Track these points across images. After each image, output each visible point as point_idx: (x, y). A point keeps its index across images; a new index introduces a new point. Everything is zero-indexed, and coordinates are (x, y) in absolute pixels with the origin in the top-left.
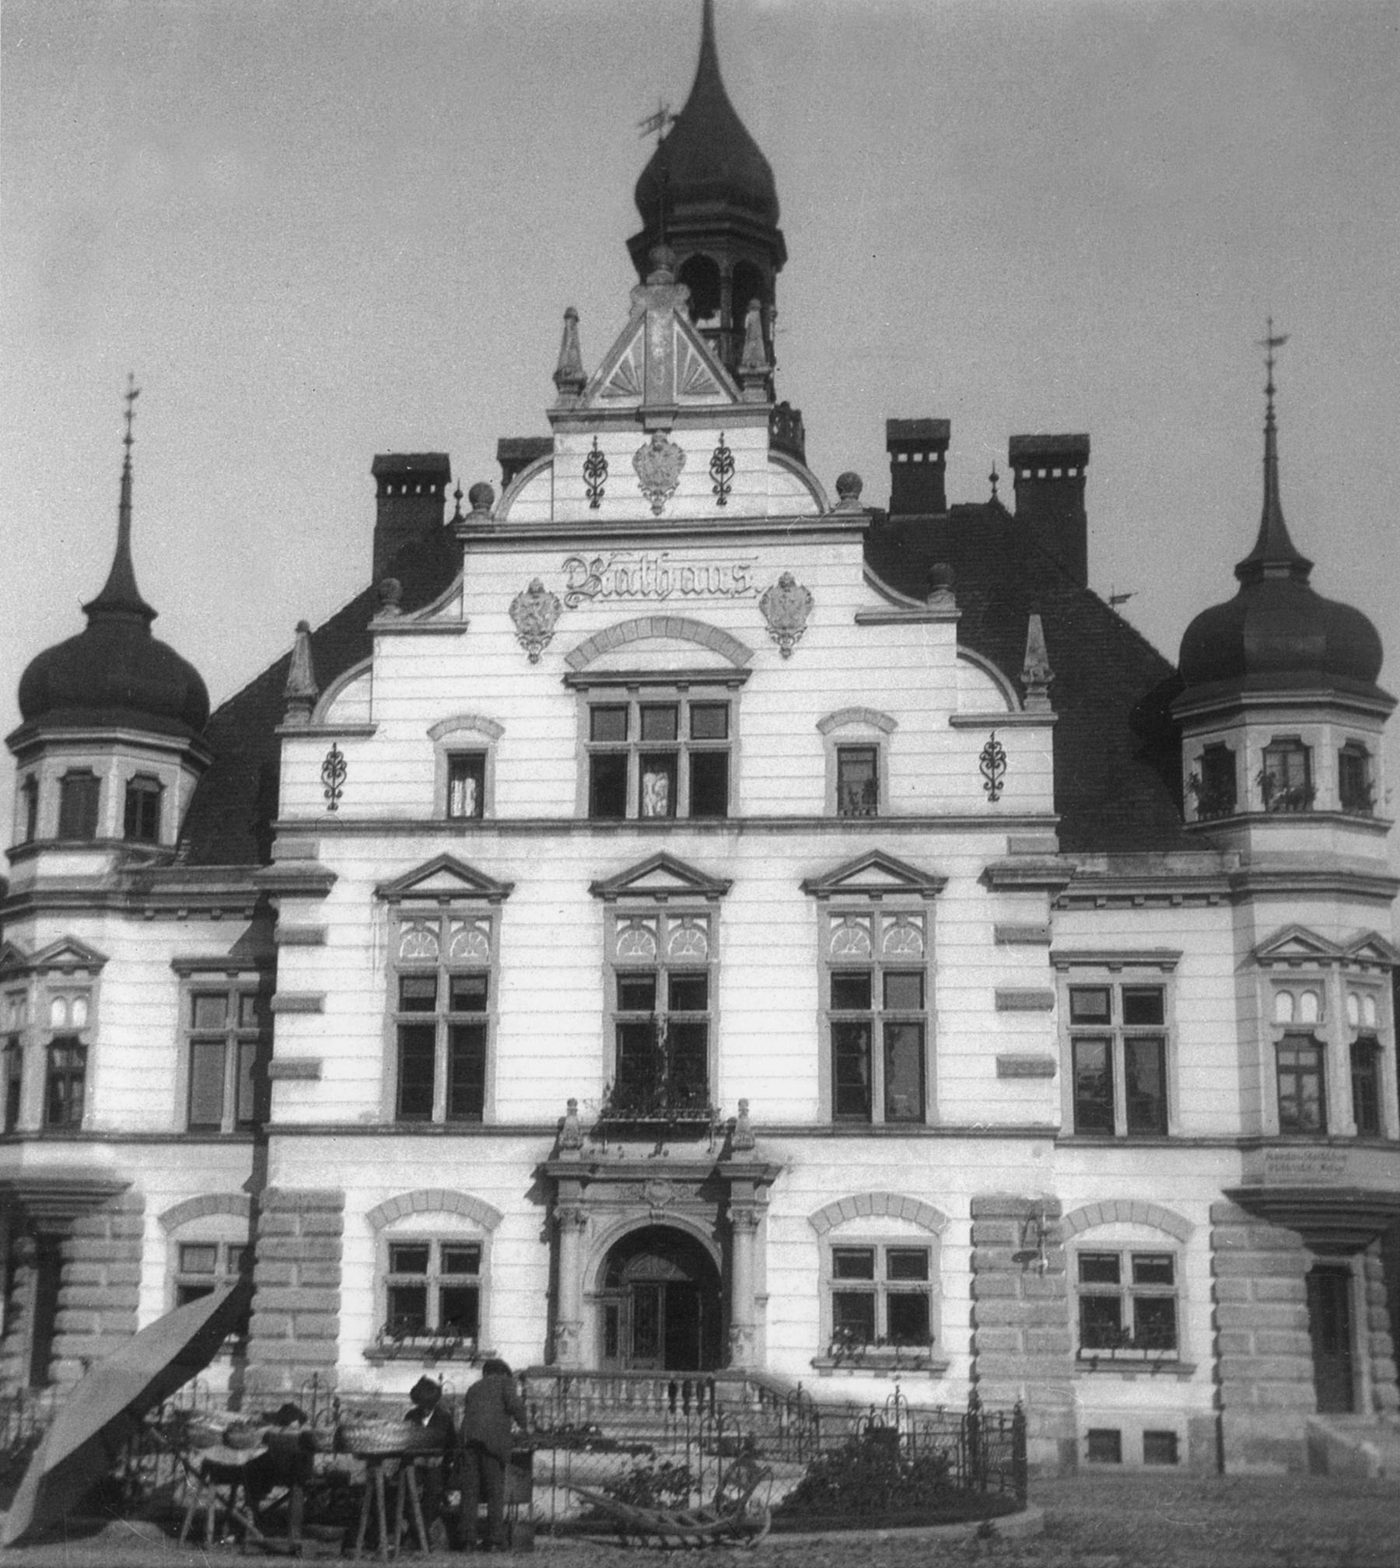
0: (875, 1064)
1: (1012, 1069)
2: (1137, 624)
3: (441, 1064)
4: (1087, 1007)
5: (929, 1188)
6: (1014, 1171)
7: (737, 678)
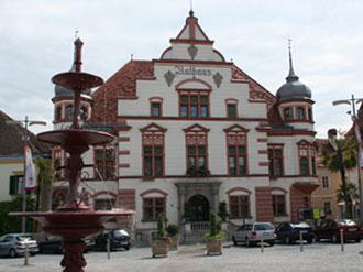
0: (239, 170)
1: (261, 164)
2: (110, 76)
3: (153, 160)
4: (270, 152)
5: (248, 185)
6: (265, 182)
7: (210, 91)
